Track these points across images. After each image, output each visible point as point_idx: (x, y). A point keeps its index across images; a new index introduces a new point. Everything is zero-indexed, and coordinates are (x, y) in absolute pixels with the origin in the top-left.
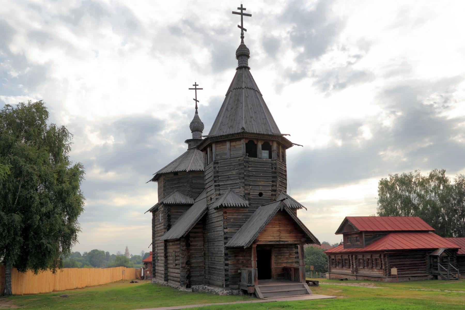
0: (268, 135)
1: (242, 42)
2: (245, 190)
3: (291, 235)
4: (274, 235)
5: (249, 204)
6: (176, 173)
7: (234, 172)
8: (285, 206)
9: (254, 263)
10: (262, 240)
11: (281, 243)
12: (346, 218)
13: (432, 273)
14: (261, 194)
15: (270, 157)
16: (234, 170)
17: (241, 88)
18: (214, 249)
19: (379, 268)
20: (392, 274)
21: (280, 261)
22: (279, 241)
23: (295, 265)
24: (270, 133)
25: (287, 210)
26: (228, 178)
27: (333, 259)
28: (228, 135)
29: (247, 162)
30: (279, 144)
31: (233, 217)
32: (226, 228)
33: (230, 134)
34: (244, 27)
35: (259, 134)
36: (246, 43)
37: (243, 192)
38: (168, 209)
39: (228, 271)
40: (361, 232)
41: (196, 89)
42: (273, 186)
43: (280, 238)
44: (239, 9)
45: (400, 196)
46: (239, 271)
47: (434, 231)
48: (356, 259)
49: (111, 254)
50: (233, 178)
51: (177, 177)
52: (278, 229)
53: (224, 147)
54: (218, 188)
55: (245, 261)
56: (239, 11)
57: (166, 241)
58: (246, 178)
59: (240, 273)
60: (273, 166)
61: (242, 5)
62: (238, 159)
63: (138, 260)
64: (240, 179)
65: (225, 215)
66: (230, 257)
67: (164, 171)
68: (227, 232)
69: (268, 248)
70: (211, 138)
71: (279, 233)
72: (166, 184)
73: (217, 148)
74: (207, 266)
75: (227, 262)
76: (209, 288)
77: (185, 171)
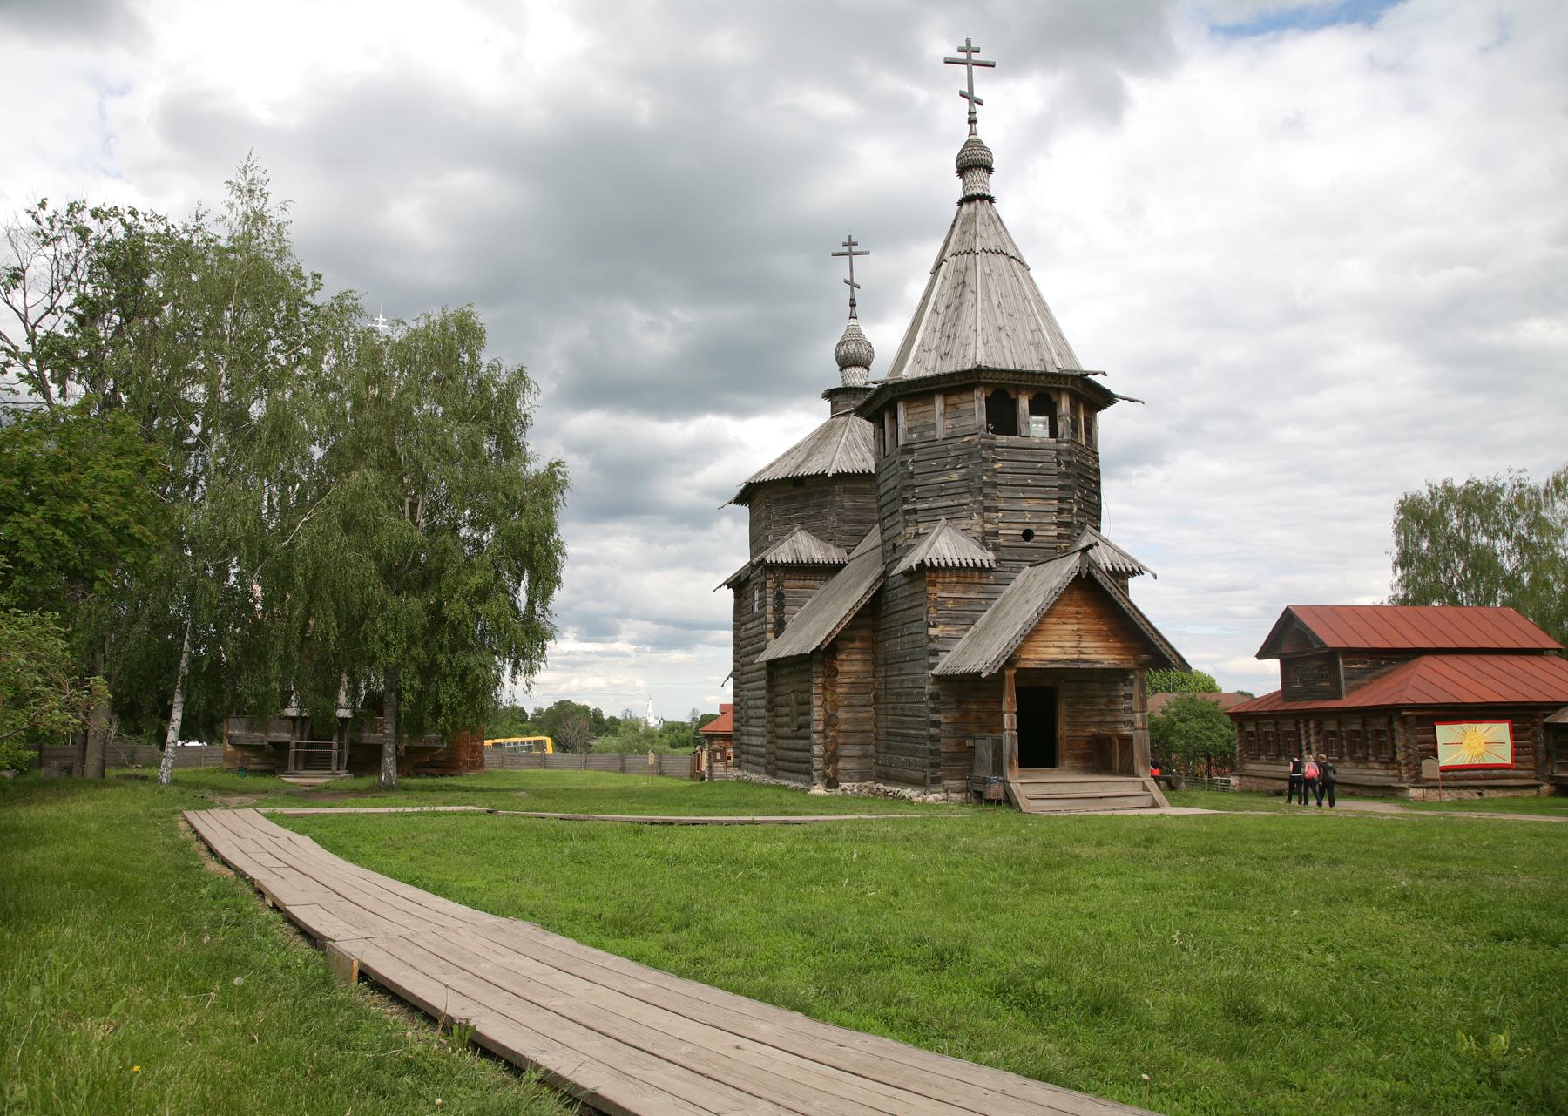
0: (1046, 374)
3: (1112, 644)
4: (1072, 644)
5: (997, 561)
6: (797, 482)
7: (955, 476)
8: (1093, 564)
9: (1009, 720)
11: (1083, 666)
13: (1551, 778)
14: (1028, 535)
15: (1053, 433)
17: (971, 252)
18: (902, 682)
19: (1385, 757)
20: (1424, 776)
21: (1082, 719)
22: (1078, 660)
23: (1126, 731)
24: (1051, 369)
25: (1098, 576)
26: (939, 491)
27: (1251, 734)
28: (938, 376)
29: (991, 447)
30: (1076, 399)
32: (935, 626)
33: (945, 375)
34: (977, 94)
35: (1021, 373)
40: (1335, 652)
41: (851, 254)
42: (1060, 511)
45: (1462, 547)
46: (969, 743)
47: (1559, 650)
48: (1317, 733)
49: (606, 716)
51: (801, 491)
52: (1075, 627)
53: (930, 408)
55: (984, 716)
56: (963, 56)
57: (773, 664)
58: (987, 490)
59: (972, 748)
60: (1062, 459)
63: (683, 735)
66: (945, 703)
67: (767, 477)
70: (895, 385)
74: (882, 731)
76: (888, 788)
77: (824, 474)
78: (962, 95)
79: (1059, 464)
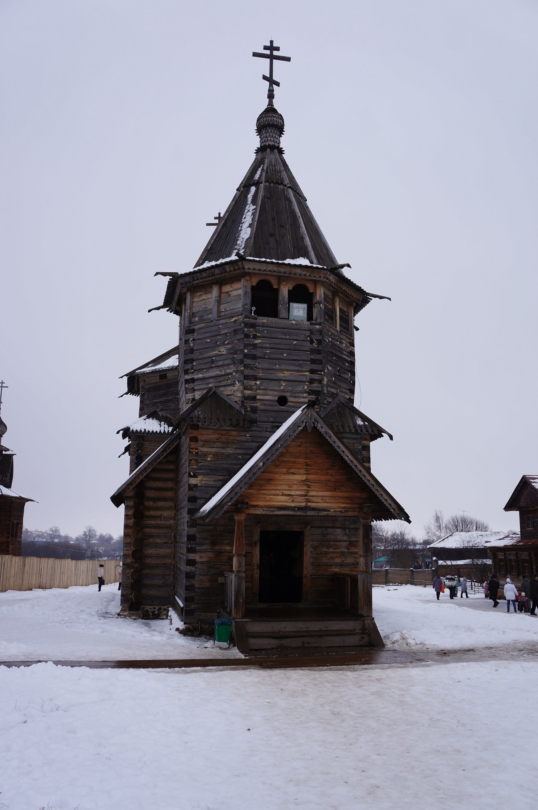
1: (271, 103)
2: (245, 389)
4: (288, 493)
7: (223, 350)
10: (261, 503)
11: (310, 513)
12: (524, 477)
15: (310, 317)
16: (224, 344)
26: (212, 363)
27: (501, 560)
29: (253, 326)
31: (213, 450)
32: (195, 476)
36: (277, 105)
37: (240, 395)
38: (138, 444)
39: (193, 577)
42: (312, 381)
43: (308, 501)
44: (266, 48)
46: (221, 580)
50: (221, 363)
52: (304, 477)
53: (209, 296)
54: (190, 386)
56: (268, 52)
60: (314, 338)
61: (272, 42)
62: (233, 320)
64: (234, 363)
65: (193, 445)
66: (200, 544)
68: (196, 486)
69: (296, 528)
71: (305, 488)
72: (146, 397)
73: (196, 300)
75: (192, 556)
78: (264, 78)
79: (312, 342)
